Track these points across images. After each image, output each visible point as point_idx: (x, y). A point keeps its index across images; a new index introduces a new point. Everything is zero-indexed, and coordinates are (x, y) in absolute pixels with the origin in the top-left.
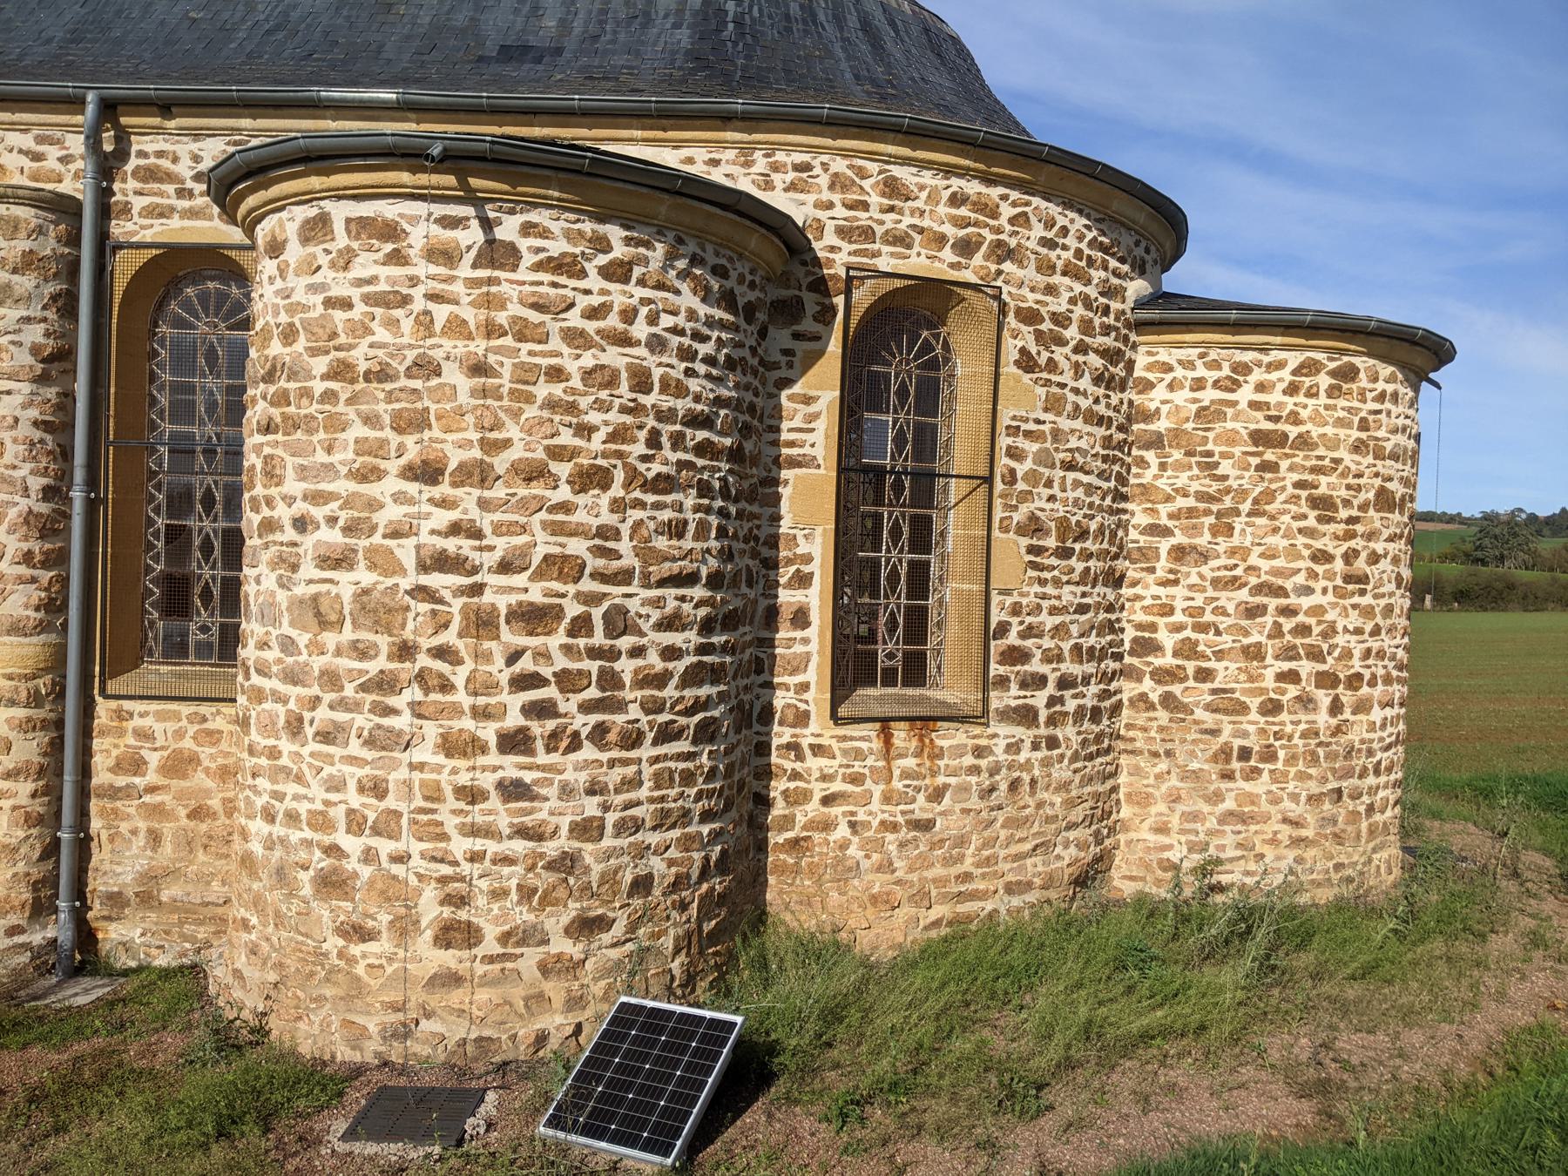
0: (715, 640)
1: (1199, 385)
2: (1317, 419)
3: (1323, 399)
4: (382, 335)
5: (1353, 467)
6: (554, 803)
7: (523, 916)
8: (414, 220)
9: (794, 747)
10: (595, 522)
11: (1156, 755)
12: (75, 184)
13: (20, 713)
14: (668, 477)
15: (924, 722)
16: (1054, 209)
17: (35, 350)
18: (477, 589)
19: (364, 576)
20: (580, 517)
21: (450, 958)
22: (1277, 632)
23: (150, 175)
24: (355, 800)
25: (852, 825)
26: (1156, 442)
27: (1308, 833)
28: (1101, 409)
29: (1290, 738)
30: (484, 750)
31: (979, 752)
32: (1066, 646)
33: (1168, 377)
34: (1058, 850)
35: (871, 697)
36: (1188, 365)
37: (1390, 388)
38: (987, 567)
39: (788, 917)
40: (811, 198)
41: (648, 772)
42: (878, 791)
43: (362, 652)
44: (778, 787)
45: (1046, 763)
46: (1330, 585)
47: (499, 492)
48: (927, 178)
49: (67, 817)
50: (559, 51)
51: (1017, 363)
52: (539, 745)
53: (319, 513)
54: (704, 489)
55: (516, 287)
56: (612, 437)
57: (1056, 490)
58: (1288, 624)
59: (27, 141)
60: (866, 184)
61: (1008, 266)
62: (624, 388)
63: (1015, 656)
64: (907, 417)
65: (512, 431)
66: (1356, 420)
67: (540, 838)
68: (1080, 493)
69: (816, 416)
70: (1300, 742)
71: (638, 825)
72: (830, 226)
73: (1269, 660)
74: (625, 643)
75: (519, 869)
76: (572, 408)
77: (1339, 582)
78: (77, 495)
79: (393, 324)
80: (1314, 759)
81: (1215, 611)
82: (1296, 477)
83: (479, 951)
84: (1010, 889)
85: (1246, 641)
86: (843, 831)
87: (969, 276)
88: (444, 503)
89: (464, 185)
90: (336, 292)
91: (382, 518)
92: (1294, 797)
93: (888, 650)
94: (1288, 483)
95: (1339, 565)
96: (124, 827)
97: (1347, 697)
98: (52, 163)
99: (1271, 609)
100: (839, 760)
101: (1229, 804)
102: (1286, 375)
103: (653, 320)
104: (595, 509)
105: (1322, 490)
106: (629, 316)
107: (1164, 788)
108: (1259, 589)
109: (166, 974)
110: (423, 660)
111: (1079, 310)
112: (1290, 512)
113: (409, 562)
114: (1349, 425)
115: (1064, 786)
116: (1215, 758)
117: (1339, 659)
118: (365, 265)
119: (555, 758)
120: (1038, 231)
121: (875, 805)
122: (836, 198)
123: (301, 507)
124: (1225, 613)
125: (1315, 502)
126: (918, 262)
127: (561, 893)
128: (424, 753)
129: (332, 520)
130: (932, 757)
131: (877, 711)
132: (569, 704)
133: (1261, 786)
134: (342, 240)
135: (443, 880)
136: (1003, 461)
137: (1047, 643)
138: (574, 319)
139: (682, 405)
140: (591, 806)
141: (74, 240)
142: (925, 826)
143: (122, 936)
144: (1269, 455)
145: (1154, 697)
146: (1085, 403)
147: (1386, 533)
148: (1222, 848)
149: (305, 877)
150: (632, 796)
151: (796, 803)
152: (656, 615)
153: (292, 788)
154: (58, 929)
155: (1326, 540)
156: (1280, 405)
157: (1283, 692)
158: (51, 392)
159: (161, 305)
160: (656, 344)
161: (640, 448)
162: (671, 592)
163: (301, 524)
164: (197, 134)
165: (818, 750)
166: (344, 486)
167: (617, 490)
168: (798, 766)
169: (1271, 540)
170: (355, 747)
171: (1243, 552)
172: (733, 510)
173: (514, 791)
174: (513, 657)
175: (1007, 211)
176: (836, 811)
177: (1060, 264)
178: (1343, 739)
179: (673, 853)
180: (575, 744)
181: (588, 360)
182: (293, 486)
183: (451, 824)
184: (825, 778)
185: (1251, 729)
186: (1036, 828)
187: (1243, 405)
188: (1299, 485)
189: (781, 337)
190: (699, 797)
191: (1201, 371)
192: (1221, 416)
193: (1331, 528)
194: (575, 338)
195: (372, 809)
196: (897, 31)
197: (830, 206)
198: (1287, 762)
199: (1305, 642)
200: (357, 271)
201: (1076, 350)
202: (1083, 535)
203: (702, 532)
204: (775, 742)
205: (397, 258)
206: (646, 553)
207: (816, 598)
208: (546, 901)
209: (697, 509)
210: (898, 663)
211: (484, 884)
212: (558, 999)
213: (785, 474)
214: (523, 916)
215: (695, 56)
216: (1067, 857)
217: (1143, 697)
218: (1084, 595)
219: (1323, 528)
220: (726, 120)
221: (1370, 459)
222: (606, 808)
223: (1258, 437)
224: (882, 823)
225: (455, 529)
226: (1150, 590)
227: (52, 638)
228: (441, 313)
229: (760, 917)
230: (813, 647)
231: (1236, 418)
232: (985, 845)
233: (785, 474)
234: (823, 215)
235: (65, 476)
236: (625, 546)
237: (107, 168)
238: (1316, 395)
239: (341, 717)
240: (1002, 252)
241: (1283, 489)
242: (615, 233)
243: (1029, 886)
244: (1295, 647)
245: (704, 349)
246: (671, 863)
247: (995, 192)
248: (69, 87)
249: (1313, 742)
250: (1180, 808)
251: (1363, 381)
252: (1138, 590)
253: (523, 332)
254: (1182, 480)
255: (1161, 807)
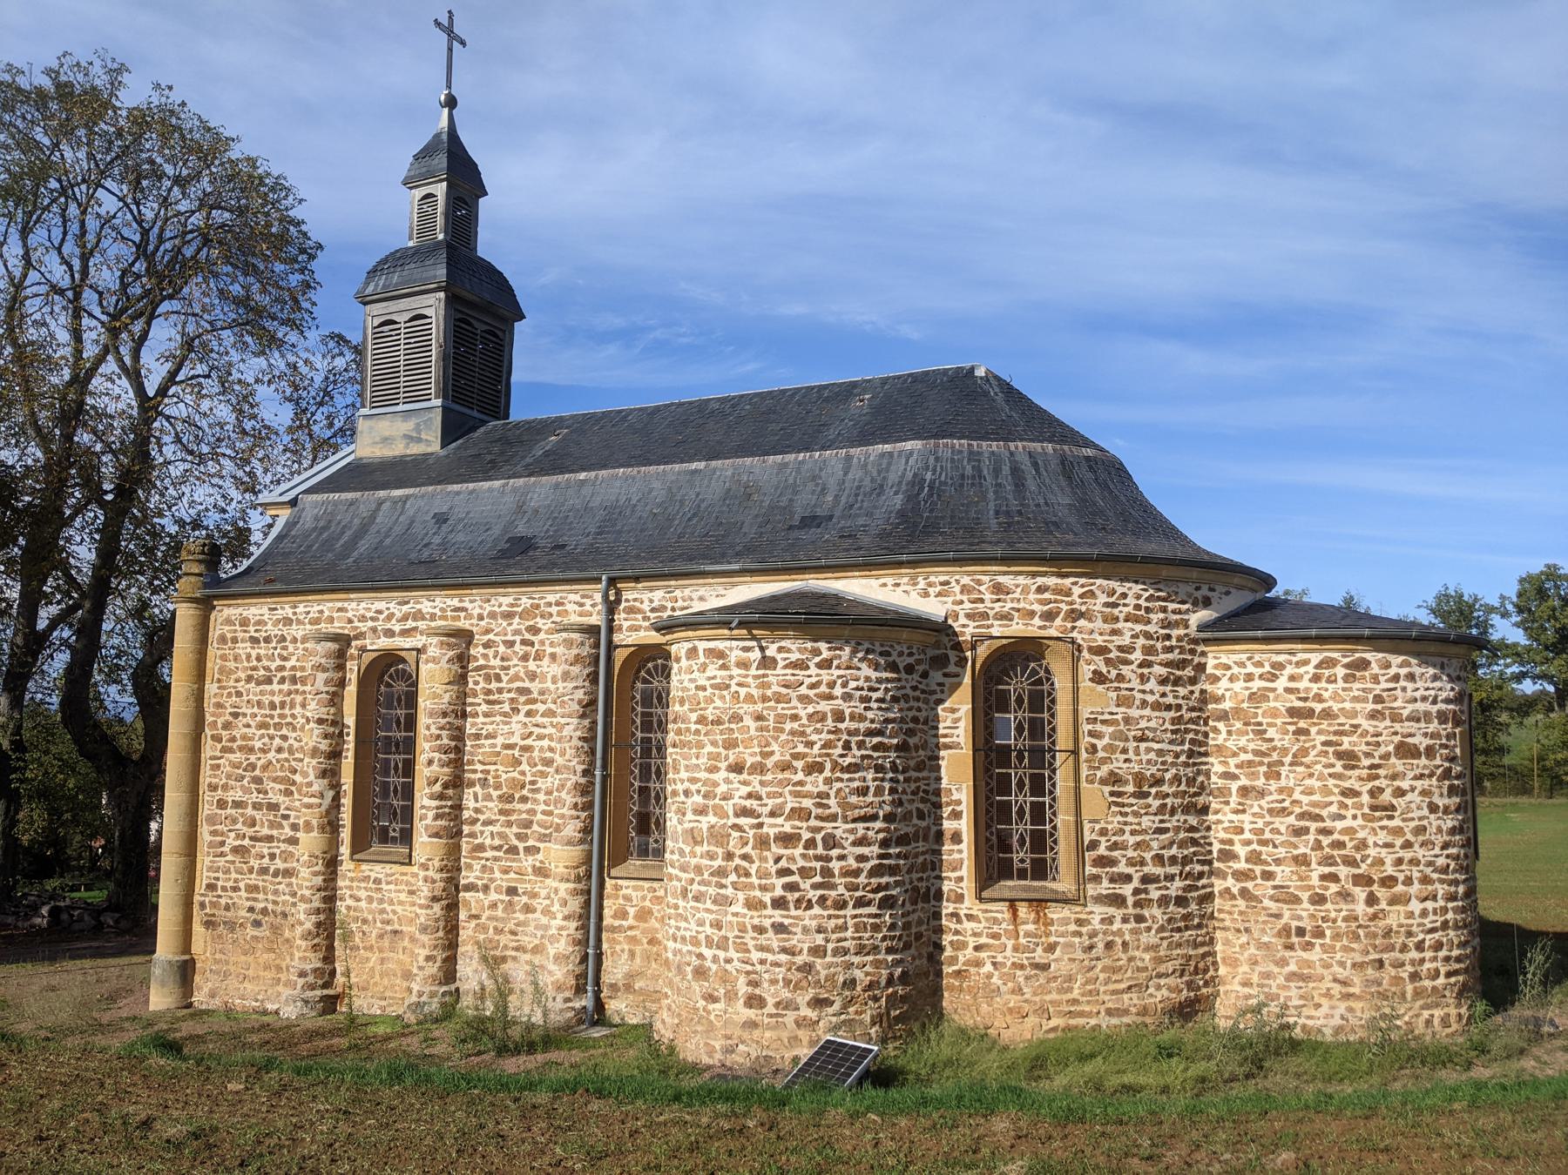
0: (891, 851)
1: (1249, 677)
2: (1335, 697)
3: (1341, 684)
4: (718, 703)
5: (1371, 730)
6: (799, 936)
7: (786, 994)
8: (731, 649)
9: (955, 915)
10: (816, 790)
11: (1238, 931)
12: (597, 619)
13: (571, 886)
14: (856, 764)
15: (1039, 903)
16: (1113, 584)
17: (580, 702)
18: (760, 825)
19: (712, 819)
20: (808, 788)
21: (751, 1014)
22: (1318, 846)
23: (631, 610)
24: (709, 930)
25: (994, 964)
26: (1224, 716)
27: (1356, 990)
28: (1170, 700)
29: (1334, 921)
30: (765, 907)
31: (1080, 922)
32: (1148, 856)
33: (1229, 673)
34: (1151, 990)
35: (1009, 886)
36: (1242, 665)
37: (1403, 671)
38: (1087, 805)
39: (956, 1017)
40: (950, 599)
41: (850, 922)
42: (1010, 944)
43: (712, 857)
44: (947, 939)
45: (1134, 932)
46: (1359, 813)
47: (769, 777)
48: (1021, 580)
49: (592, 942)
50: (831, 517)
51: (1091, 680)
52: (791, 905)
53: (693, 788)
54: (879, 769)
55: (775, 676)
56: (824, 747)
57: (1131, 755)
58: (1326, 841)
59: (577, 598)
60: (982, 588)
61: (1081, 623)
62: (830, 721)
63: (1101, 862)
64: (1024, 715)
65: (775, 747)
66: (1371, 697)
67: (793, 954)
68: (1152, 756)
69: (958, 720)
70: (1344, 925)
71: (846, 952)
72: (962, 614)
73: (1314, 865)
74: (835, 852)
75: (783, 969)
76: (803, 734)
77: (1366, 810)
78: (598, 773)
79: (722, 698)
80: (1357, 937)
81: (1272, 831)
82: (1323, 738)
83: (765, 1011)
84: (1109, 1012)
85: (1296, 852)
86: (988, 968)
87: (1053, 633)
88: (745, 783)
89: (750, 633)
90: (700, 683)
91: (719, 791)
92: (1342, 964)
93: (1021, 856)
94: (1318, 743)
95: (1365, 798)
96: (618, 948)
97: (1381, 893)
98: (588, 608)
99: (1312, 830)
100: (984, 924)
101: (1293, 967)
102: (1310, 669)
103: (844, 685)
104: (815, 783)
105: (1346, 746)
106: (832, 685)
107: (1246, 955)
108: (1302, 816)
109: (636, 1027)
110: (737, 861)
111: (1141, 641)
112: (1321, 764)
113: (731, 813)
114: (1365, 700)
115: (1155, 948)
116: (1279, 934)
117: (1372, 865)
118: (712, 670)
119: (799, 912)
120: (1103, 598)
121: (1009, 952)
122: (965, 598)
123: (687, 785)
124: (1279, 833)
125: (1340, 755)
126: (1018, 628)
127: (804, 984)
128: (738, 907)
129: (699, 792)
130: (1046, 925)
131: (1007, 895)
132: (806, 885)
133: (1315, 955)
134: (702, 659)
135: (748, 973)
136: (1086, 740)
137: (1130, 853)
138: (803, 690)
139: (863, 726)
140: (819, 939)
141: (597, 645)
142: (1045, 967)
143: (617, 1006)
144: (1302, 724)
145: (1235, 891)
146: (1150, 698)
147: (1411, 774)
148: (1290, 998)
149: (689, 969)
150: (842, 935)
151: (958, 949)
152: (852, 838)
153: (683, 924)
154: (587, 1001)
155: (1352, 781)
156: (1307, 690)
157: (1326, 889)
158: (586, 722)
159: (639, 671)
160: (847, 697)
161: (839, 751)
162: (861, 825)
163: (687, 793)
164: (651, 590)
165: (970, 917)
166: (703, 775)
167: (827, 773)
168: (958, 927)
169: (1308, 782)
170: (709, 905)
171: (1289, 791)
172: (901, 778)
173: (780, 928)
174: (777, 860)
175: (1077, 591)
176: (983, 955)
177: (1122, 616)
178: (1381, 924)
179: (867, 968)
180: (810, 906)
181: (810, 709)
182: (684, 775)
183: (751, 944)
184: (975, 934)
185: (1304, 914)
186: (1129, 974)
187: (1280, 691)
188: (1325, 744)
189: (937, 676)
190: (884, 939)
191: (1250, 669)
192: (1266, 699)
193: (1356, 772)
194: (804, 699)
195: (716, 935)
196: (1037, 470)
197: (962, 602)
198: (1333, 938)
199: (1339, 852)
200: (709, 673)
201: (1140, 666)
202: (1159, 782)
203: (879, 791)
204: (944, 912)
205: (724, 667)
206: (844, 805)
207: (965, 825)
208: (796, 987)
209: (875, 780)
210: (1027, 865)
211: (766, 976)
212: (805, 1041)
213: (942, 753)
214: (786, 994)
215: (902, 514)
216: (1161, 994)
217: (1228, 890)
218: (1162, 821)
219: (1350, 773)
220: (900, 564)
221: (1388, 723)
222: (827, 941)
223: (1293, 712)
224: (1014, 964)
225: (750, 796)
226: (1227, 817)
227: (586, 847)
228: (743, 691)
229: (939, 1014)
230: (965, 855)
231: (1276, 699)
232: (1087, 983)
233: (942, 753)
234: (957, 608)
235: (592, 763)
236: (832, 802)
237: (611, 608)
238: (1335, 681)
239: (703, 889)
240: (1074, 615)
241: (1314, 747)
242: (823, 646)
243: (1126, 1012)
244: (1332, 857)
245: (875, 695)
246: (867, 974)
247: (1068, 581)
248: (595, 574)
249: (1354, 925)
250: (1258, 969)
251: (1375, 669)
252: (1219, 816)
253: (779, 698)
254: (1243, 742)
255: (1245, 968)
